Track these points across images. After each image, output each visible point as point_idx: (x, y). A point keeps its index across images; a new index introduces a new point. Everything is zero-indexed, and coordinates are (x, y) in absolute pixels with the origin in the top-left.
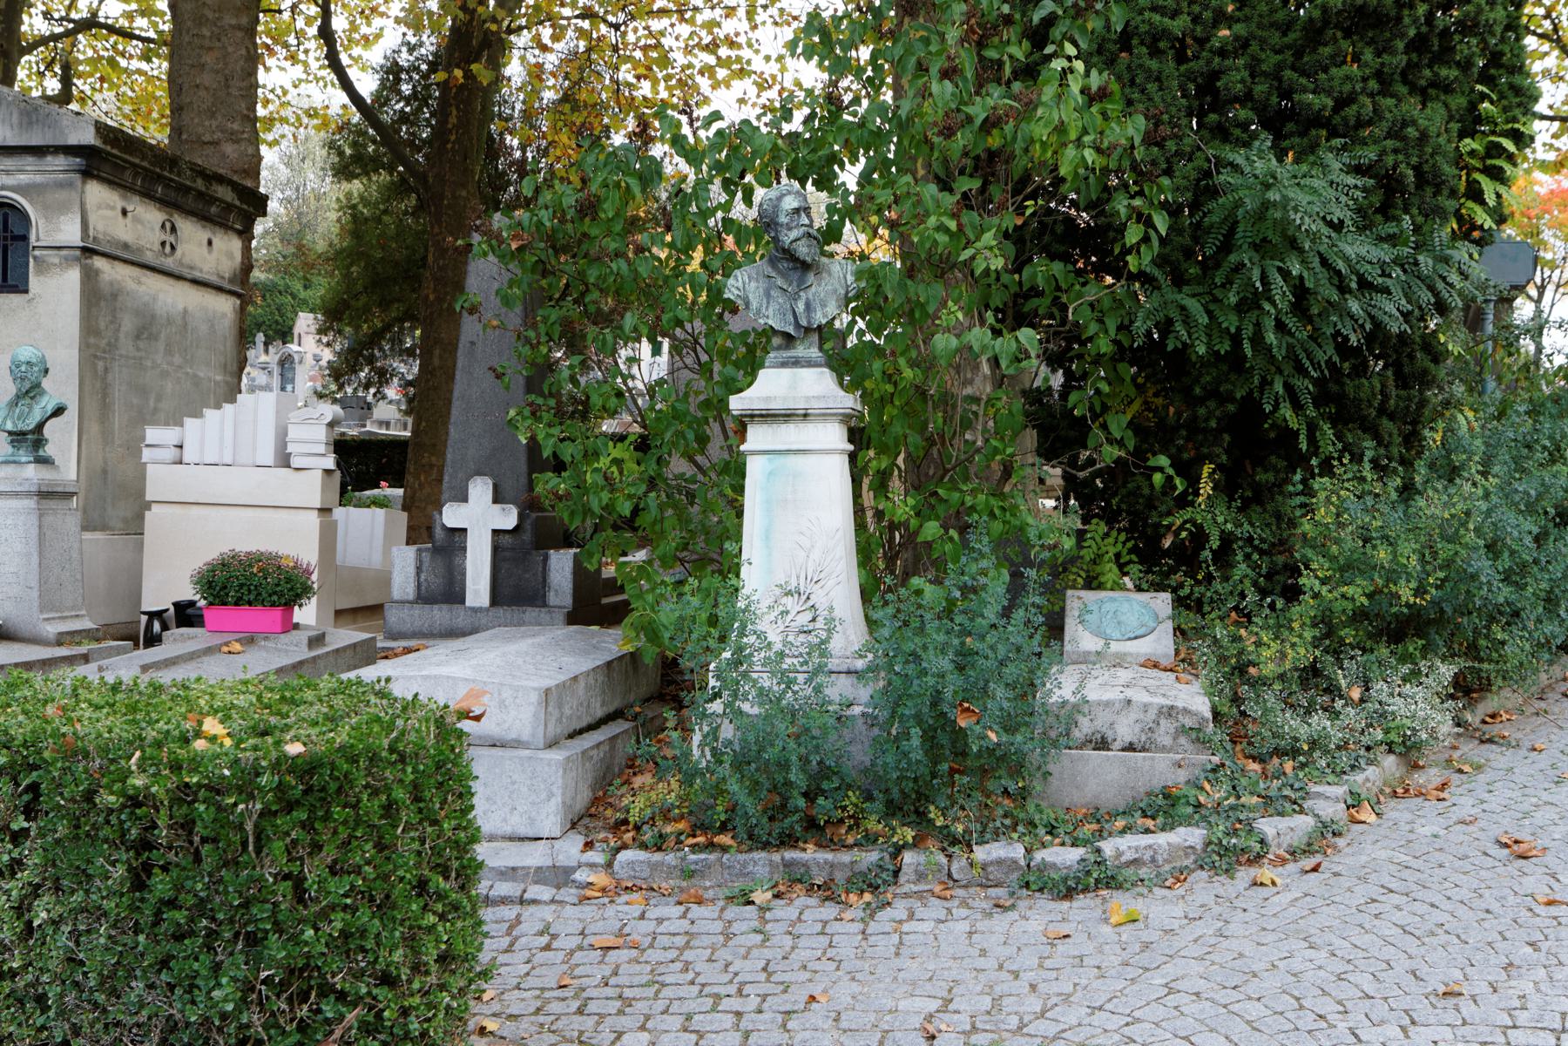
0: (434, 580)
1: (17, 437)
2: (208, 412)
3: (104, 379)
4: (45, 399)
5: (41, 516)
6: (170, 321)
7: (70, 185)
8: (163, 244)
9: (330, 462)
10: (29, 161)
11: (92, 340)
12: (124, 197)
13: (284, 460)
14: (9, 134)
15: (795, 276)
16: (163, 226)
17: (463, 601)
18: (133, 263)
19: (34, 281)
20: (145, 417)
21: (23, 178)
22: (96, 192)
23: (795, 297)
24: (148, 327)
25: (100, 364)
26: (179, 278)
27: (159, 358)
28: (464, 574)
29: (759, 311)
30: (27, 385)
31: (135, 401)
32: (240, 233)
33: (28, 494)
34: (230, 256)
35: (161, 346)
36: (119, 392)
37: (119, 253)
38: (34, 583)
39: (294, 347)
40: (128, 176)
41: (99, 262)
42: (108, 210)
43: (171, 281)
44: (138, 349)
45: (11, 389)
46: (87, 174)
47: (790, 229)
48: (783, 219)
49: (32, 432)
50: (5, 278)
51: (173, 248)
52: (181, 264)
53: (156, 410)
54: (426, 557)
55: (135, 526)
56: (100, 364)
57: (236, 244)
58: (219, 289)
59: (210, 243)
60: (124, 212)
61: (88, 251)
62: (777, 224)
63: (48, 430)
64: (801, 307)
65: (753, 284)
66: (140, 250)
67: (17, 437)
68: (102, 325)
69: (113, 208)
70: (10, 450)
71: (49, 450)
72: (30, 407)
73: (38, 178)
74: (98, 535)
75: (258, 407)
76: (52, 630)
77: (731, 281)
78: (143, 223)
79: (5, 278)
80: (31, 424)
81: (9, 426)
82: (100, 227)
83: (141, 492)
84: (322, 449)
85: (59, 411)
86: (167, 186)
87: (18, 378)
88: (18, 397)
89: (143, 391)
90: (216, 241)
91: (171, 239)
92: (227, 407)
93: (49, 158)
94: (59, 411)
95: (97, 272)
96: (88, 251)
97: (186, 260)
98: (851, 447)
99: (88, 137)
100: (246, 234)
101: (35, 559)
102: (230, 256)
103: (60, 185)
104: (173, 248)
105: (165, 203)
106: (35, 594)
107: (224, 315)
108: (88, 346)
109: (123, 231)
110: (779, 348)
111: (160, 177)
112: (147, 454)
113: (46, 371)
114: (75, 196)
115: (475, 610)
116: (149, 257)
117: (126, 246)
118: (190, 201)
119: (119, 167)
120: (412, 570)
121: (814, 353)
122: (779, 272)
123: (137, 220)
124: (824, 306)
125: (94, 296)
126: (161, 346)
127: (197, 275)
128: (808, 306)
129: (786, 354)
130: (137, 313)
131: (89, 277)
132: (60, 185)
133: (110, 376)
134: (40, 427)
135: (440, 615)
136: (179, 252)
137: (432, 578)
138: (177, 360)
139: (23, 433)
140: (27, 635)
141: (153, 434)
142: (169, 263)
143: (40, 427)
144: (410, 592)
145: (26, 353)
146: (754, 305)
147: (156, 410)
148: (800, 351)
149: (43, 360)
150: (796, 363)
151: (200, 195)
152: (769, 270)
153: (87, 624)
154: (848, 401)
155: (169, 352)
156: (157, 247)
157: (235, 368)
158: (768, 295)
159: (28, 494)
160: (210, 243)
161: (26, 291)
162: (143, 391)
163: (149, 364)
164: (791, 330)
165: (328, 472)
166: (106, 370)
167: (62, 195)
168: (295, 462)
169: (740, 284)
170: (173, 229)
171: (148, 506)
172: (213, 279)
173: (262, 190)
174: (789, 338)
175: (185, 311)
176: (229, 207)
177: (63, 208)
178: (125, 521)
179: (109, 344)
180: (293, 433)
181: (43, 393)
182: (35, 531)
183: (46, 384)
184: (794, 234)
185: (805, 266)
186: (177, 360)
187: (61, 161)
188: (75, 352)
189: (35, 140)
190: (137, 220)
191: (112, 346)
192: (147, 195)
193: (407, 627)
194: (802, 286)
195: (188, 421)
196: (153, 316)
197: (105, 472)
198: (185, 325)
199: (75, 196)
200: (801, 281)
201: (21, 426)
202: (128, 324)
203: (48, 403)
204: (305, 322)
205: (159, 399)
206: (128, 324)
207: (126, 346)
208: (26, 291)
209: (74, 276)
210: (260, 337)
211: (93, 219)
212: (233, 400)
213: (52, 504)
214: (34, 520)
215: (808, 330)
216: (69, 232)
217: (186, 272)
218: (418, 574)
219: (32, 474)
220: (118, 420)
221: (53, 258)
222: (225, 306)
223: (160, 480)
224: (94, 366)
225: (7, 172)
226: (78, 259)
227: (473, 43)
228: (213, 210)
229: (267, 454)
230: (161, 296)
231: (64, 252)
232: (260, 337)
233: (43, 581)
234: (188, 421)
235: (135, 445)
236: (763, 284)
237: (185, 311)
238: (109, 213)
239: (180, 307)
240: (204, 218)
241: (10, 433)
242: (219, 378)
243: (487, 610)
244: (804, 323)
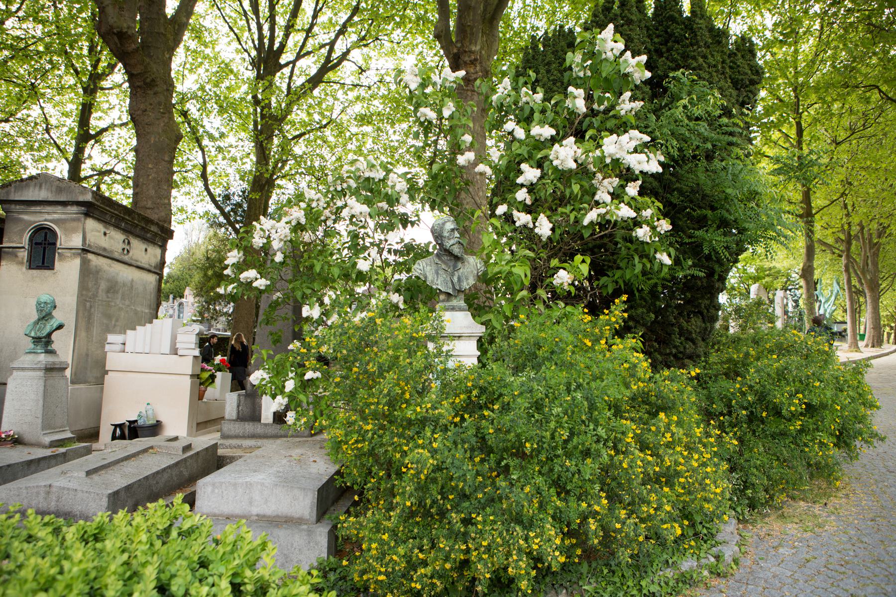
0: (246, 410)
1: (37, 340)
2: (138, 328)
3: (89, 311)
4: (54, 320)
5: (46, 380)
6: (124, 285)
7: (78, 220)
8: (123, 249)
9: (197, 352)
10: (59, 209)
11: (84, 292)
12: (105, 227)
13: (174, 351)
14: (50, 195)
15: (451, 264)
16: (124, 241)
17: (260, 420)
18: (108, 257)
19: (57, 264)
20: (109, 330)
21: (56, 216)
22: (91, 224)
23: (453, 275)
24: (113, 287)
25: (88, 304)
26: (130, 265)
27: (118, 302)
28: (260, 407)
29: (432, 281)
30: (44, 314)
31: (105, 321)
32: (160, 247)
33: (40, 369)
34: (155, 256)
35: (119, 295)
36: (97, 316)
37: (101, 252)
38: (40, 416)
39: (183, 300)
40: (108, 217)
41: (90, 256)
42: (95, 231)
43: (126, 266)
44: (108, 297)
45: (35, 316)
46: (87, 215)
47: (450, 239)
48: (446, 234)
49: (45, 337)
50: (43, 263)
51: (128, 251)
52: (131, 259)
53: (115, 325)
54: (242, 398)
55: (100, 382)
56: (88, 304)
57: (158, 251)
58: (149, 271)
59: (146, 250)
60: (105, 234)
61: (85, 251)
62: (442, 237)
63: (54, 336)
64: (455, 279)
65: (429, 268)
66: (112, 252)
67: (37, 340)
68: (90, 285)
69: (99, 232)
70: (32, 346)
71: (54, 346)
72: (45, 325)
73: (63, 216)
74: (82, 386)
75: (163, 325)
76: (47, 440)
77: (416, 266)
78: (115, 240)
79: (43, 263)
80: (45, 333)
81: (33, 334)
82: (92, 240)
83: (104, 366)
84: (193, 346)
85: (60, 327)
86: (127, 223)
87: (39, 310)
88: (39, 320)
89: (109, 317)
90: (149, 250)
91: (127, 247)
92: (148, 325)
93: (69, 207)
94: (60, 327)
95: (89, 261)
96: (85, 251)
97: (134, 257)
98: (479, 353)
99: (89, 197)
100: (163, 248)
101: (41, 403)
102: (155, 256)
103: (74, 220)
104: (128, 251)
105: (125, 231)
106: (40, 421)
107: (151, 283)
108: (82, 295)
109: (104, 242)
110: (443, 301)
111: (123, 219)
112: (107, 348)
113: (55, 307)
114: (81, 225)
115: (266, 425)
116: (116, 255)
117: (105, 249)
118: (138, 231)
119: (104, 213)
120: (235, 405)
121: (462, 303)
122: (443, 261)
123: (111, 238)
124: (467, 279)
125: (86, 272)
126: (119, 295)
127: (139, 264)
128: (459, 279)
129: (447, 304)
130: (108, 280)
131: (85, 263)
132: (74, 220)
133: (93, 310)
134: (49, 335)
135: (249, 427)
136: (131, 254)
137: (245, 409)
138: (127, 302)
139: (40, 338)
140: (33, 440)
141: (111, 338)
142: (126, 258)
143: (49, 335)
144: (234, 415)
145: (44, 298)
146: (430, 278)
147: (115, 325)
148: (455, 302)
149: (54, 302)
150: (453, 309)
151: (143, 228)
152: (437, 260)
153: (69, 435)
154: (481, 330)
155: (123, 298)
156: (120, 250)
157: (155, 306)
158: (437, 273)
159: (40, 369)
160: (146, 250)
161: (53, 269)
162: (109, 317)
163: (113, 304)
164: (450, 291)
165: (195, 357)
166: (91, 307)
167: (74, 224)
168: (180, 352)
169: (421, 267)
170: (129, 243)
171: (106, 372)
172: (146, 266)
173: (172, 228)
174: (448, 294)
175: (132, 280)
176: (156, 234)
177: (74, 231)
178: (96, 378)
179: (93, 294)
180: (180, 338)
181: (52, 317)
182: (42, 388)
183: (54, 313)
184: (452, 242)
185: (457, 258)
186: (127, 302)
187: (75, 209)
188: (75, 298)
189: (62, 198)
190: (111, 238)
191: (95, 296)
192: (117, 227)
193: (232, 433)
194: (455, 269)
195: (129, 332)
196: (117, 282)
197: (87, 355)
198: (132, 287)
199: (81, 225)
200: (455, 266)
201: (39, 334)
202: (103, 285)
203: (54, 323)
204: (188, 292)
205: (117, 320)
206: (103, 285)
207: (102, 295)
208: (53, 269)
209: (78, 261)
210: (171, 296)
211: (88, 236)
212: (151, 322)
213: (54, 374)
214: (42, 383)
215: (459, 291)
216: (76, 241)
217: (133, 263)
218: (238, 407)
219: (43, 358)
220: (96, 331)
221: (68, 253)
222: (152, 278)
223: (114, 360)
224: (85, 306)
225: (48, 213)
226: (79, 254)
227: (358, 3)
228: (149, 235)
229: (167, 348)
230: (121, 273)
231: (73, 251)
232: (171, 296)
233: (45, 415)
234: (129, 332)
235: (103, 342)
236: (434, 267)
237: (132, 280)
238: (98, 234)
239: (130, 278)
240: (144, 239)
241: (33, 338)
242: (147, 311)
243: (272, 425)
244: (458, 288)
